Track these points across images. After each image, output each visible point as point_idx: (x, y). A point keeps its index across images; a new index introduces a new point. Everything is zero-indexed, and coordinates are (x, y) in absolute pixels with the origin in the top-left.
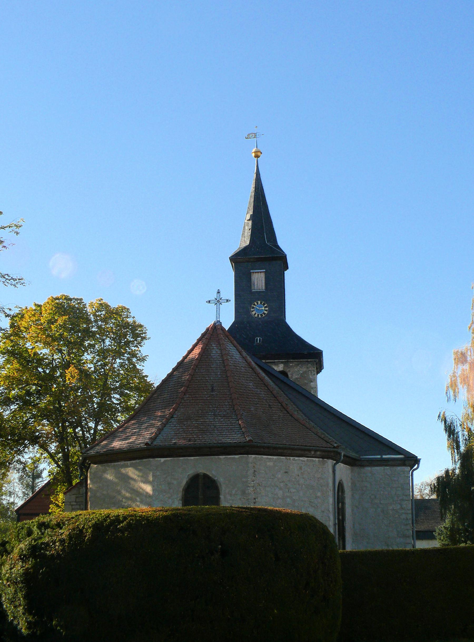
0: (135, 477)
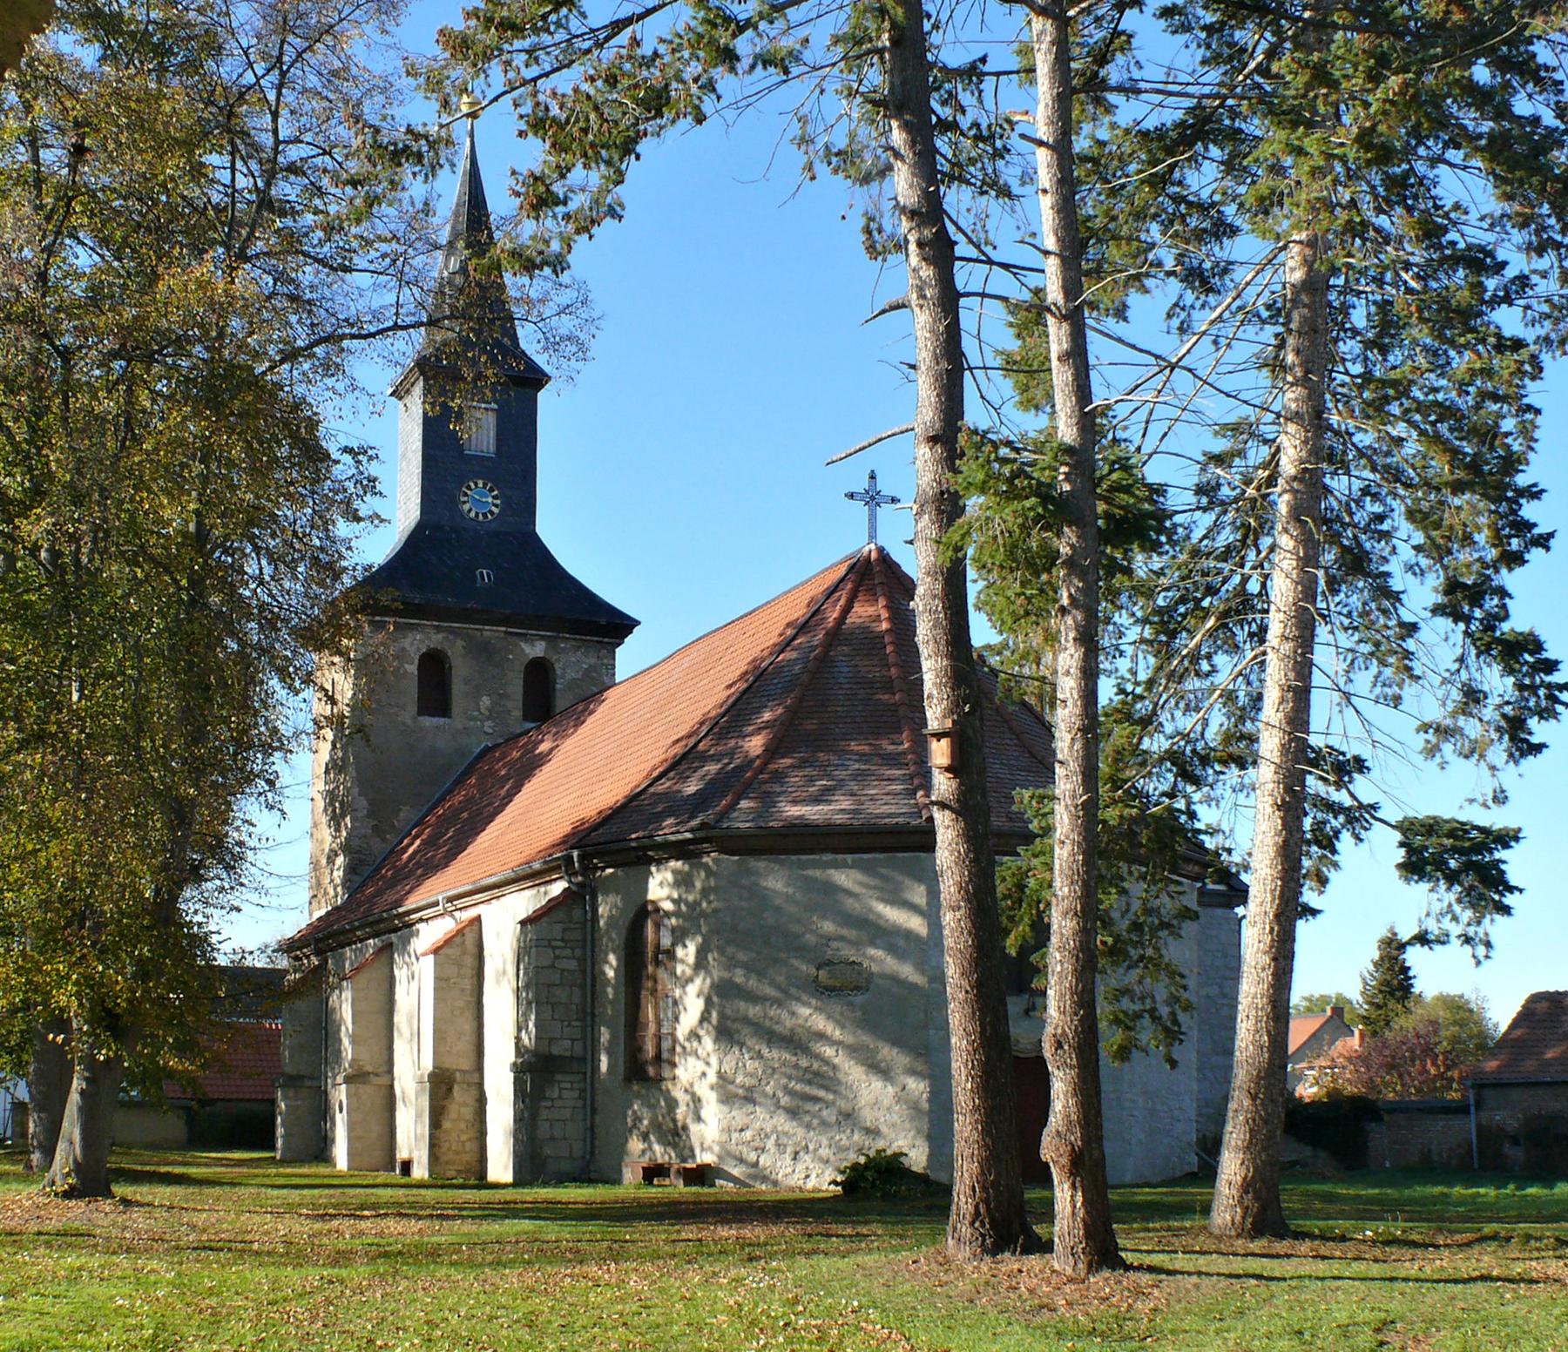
0: (857, 889)
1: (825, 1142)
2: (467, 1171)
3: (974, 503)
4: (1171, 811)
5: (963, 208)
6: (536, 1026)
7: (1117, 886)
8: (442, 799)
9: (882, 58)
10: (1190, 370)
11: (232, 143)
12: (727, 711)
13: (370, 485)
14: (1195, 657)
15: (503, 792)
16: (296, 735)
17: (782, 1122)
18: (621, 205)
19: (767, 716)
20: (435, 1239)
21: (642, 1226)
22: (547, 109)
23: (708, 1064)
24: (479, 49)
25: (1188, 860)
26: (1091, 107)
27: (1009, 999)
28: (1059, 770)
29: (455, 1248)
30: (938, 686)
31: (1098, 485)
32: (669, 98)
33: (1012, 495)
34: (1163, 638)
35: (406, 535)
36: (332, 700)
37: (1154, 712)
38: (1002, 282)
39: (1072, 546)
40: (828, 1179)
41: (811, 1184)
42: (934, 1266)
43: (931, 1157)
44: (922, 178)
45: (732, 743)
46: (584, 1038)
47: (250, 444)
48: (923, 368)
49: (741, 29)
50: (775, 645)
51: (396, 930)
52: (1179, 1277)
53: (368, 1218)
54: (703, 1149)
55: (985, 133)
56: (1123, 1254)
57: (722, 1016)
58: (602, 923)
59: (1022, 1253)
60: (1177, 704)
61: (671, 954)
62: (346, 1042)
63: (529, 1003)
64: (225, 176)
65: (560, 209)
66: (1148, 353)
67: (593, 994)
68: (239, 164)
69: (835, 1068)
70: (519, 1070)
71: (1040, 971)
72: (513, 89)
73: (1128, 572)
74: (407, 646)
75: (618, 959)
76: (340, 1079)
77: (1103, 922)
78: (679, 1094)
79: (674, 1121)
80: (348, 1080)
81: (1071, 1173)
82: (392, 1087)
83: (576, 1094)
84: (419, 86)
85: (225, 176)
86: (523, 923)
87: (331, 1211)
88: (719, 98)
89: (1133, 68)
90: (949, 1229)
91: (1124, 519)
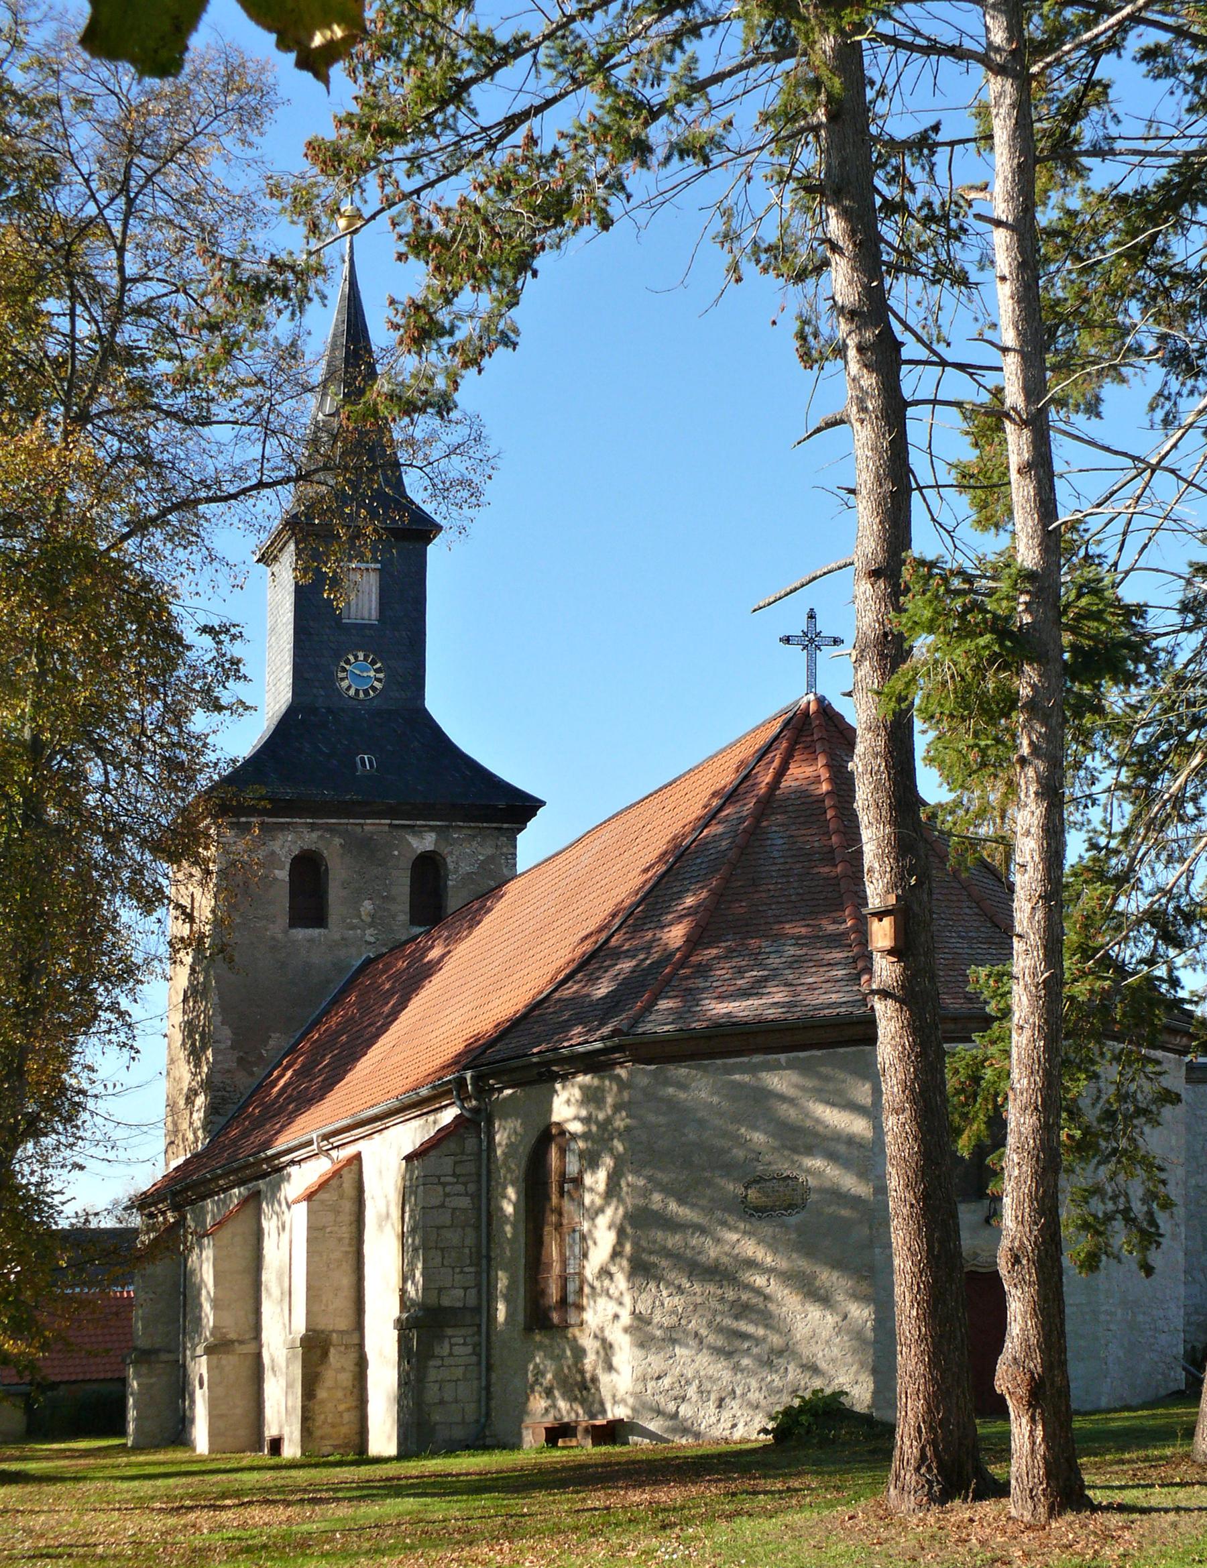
0: (791, 1092)
1: (754, 1384)
2: (346, 1445)
3: (923, 644)
4: (1150, 980)
5: (912, 300)
6: (423, 1274)
7: (1086, 1070)
8: (317, 1022)
9: (817, 137)
10: (1173, 471)
11: (71, 286)
12: (643, 899)
13: (232, 669)
14: (1178, 801)
15: (386, 1009)
16: (147, 962)
17: (706, 1364)
18: (516, 331)
19: (689, 901)
20: (305, 1527)
21: (541, 1496)
22: (430, 226)
23: (621, 1304)
24: (352, 161)
25: (1174, 1031)
26: (1061, 173)
27: (962, 1208)
28: (1018, 945)
29: (327, 1536)
30: (880, 857)
31: (1065, 613)
32: (570, 202)
33: (966, 632)
34: (1142, 781)
35: (275, 721)
36: (190, 918)
37: (1131, 869)
38: (957, 386)
39: (1034, 687)
40: (758, 1427)
41: (738, 1434)
42: (874, 1522)
43: (876, 1393)
44: (864, 272)
45: (649, 935)
46: (478, 1286)
47: (86, 635)
48: (864, 492)
49: (654, 115)
50: (699, 819)
51: (265, 1175)
52: (1154, 1515)
53: (229, 1507)
54: (615, 1402)
55: (938, 212)
56: (1090, 1493)
57: (636, 1245)
58: (499, 1152)
59: (974, 1500)
60: (1158, 856)
61: (578, 1181)
62: (207, 1307)
63: (415, 1250)
64: (63, 324)
65: (446, 341)
66: (1125, 454)
67: (489, 1234)
68: (79, 309)
69: (767, 1298)
70: (403, 1327)
71: (997, 1174)
72: (391, 205)
73: (1099, 710)
74: (278, 850)
75: (517, 1193)
76: (200, 1350)
77: (1070, 1113)
78: (588, 1343)
79: (582, 1372)
80: (209, 1351)
81: (1030, 1405)
82: (259, 1356)
83: (469, 1349)
84: (284, 209)
85: (63, 324)
86: (408, 1158)
87: (188, 1503)
88: (629, 197)
89: (1109, 123)
90: (891, 1477)
91: (1094, 650)
